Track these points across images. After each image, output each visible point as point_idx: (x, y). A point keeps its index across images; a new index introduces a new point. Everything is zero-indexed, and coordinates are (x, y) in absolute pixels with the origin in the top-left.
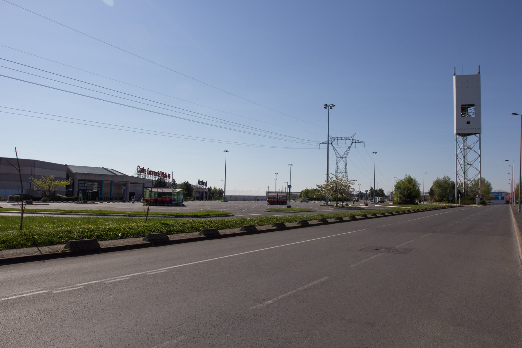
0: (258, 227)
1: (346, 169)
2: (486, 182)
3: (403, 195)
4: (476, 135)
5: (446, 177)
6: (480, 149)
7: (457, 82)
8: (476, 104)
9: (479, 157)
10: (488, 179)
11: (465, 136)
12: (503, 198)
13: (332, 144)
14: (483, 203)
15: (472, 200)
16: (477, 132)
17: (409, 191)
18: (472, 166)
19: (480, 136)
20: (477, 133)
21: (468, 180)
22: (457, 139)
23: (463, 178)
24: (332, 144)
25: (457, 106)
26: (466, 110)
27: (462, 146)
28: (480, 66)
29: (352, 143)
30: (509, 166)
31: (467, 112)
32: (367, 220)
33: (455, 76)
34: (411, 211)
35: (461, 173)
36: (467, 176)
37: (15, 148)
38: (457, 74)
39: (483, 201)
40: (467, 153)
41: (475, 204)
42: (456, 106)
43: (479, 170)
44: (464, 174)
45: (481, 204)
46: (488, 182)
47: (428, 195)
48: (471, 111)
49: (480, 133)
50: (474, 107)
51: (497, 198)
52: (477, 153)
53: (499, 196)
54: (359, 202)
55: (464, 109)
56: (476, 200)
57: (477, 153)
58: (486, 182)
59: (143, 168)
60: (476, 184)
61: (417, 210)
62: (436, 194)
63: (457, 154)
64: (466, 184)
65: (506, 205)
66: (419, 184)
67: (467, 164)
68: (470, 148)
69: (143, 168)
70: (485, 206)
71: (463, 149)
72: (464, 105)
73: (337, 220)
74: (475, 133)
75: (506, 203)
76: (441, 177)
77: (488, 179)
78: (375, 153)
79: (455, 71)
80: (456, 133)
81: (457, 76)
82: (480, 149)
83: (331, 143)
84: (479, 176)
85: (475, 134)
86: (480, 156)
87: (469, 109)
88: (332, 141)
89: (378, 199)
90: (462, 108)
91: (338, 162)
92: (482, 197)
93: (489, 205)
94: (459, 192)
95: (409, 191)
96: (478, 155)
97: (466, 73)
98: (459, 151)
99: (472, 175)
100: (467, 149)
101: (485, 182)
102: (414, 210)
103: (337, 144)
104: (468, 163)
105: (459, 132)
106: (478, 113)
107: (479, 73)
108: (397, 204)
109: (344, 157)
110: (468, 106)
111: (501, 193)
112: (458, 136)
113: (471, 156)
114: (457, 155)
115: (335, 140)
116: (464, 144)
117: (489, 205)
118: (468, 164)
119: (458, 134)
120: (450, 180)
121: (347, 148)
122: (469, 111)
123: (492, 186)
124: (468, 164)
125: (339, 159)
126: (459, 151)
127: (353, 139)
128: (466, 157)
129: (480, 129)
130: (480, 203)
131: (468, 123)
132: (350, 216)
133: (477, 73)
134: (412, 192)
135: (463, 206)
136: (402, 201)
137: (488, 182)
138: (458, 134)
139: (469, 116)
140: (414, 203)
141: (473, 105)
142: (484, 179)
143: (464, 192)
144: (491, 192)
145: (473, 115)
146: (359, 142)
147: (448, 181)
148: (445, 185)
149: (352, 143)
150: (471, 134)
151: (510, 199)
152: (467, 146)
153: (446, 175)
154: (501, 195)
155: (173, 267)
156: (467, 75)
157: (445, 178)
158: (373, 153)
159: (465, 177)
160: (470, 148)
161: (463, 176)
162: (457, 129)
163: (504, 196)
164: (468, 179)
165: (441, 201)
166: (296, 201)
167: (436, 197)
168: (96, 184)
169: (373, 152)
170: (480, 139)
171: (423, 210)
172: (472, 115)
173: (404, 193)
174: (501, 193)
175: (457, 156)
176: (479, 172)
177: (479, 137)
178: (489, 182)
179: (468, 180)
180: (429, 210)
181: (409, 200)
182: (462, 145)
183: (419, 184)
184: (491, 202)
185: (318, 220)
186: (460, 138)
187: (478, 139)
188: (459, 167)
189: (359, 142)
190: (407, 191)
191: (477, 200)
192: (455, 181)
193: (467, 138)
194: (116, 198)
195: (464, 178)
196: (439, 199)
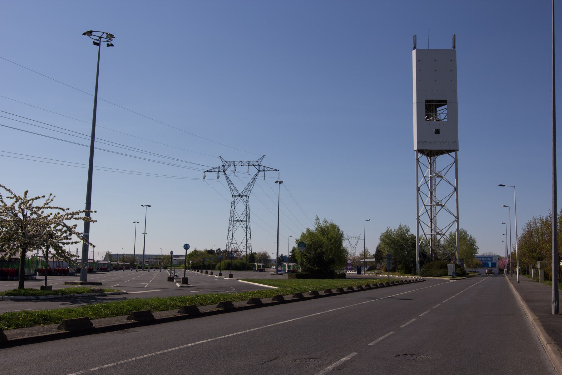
0: (321, 292)
1: (247, 215)
2: (468, 238)
5: (403, 227)
6: (457, 177)
7: (418, 60)
9: (455, 193)
10: (472, 233)
12: (494, 265)
13: (225, 173)
14: (461, 273)
15: (442, 270)
17: (318, 251)
18: (444, 207)
19: (456, 155)
20: (451, 149)
21: (438, 233)
24: (225, 173)
25: (418, 103)
26: (434, 110)
27: (427, 172)
28: (455, 36)
29: (259, 171)
30: (504, 206)
34: (363, 287)
35: (425, 219)
36: (436, 225)
38: (418, 48)
39: (462, 271)
40: (436, 186)
41: (446, 275)
43: (456, 215)
44: (431, 221)
45: (458, 275)
46: (472, 238)
47: (374, 260)
48: (442, 112)
49: (455, 151)
51: (485, 265)
52: (452, 185)
53: (488, 261)
54: (265, 272)
57: (452, 185)
58: (468, 238)
59: (172, 252)
60: (451, 241)
61: (391, 283)
63: (419, 186)
64: (434, 239)
65: (499, 278)
67: (435, 204)
68: (441, 177)
69: (172, 252)
70: (465, 281)
71: (429, 178)
73: (349, 289)
74: (448, 149)
75: (499, 274)
76: (394, 227)
78: (280, 183)
80: (416, 149)
82: (457, 177)
83: (224, 171)
84: (453, 229)
85: (449, 151)
86: (456, 190)
87: (438, 109)
88: (226, 167)
89: (289, 267)
90: (426, 104)
91: (236, 204)
92: (461, 263)
93: (473, 276)
94: (423, 254)
95: (318, 251)
96: (454, 188)
97: (434, 46)
98: (422, 181)
100: (436, 176)
102: (375, 285)
103: (234, 173)
105: (419, 149)
106: (453, 116)
107: (454, 47)
109: (245, 195)
110: (437, 102)
111: (492, 258)
112: (419, 155)
114: (419, 187)
115: (230, 165)
116: (431, 169)
117: (473, 276)
118: (438, 204)
119: (420, 151)
121: (249, 180)
123: (478, 244)
124: (438, 204)
125: (236, 198)
126: (422, 181)
127: (259, 165)
129: (456, 142)
130: (454, 275)
131: (437, 132)
132: (221, 303)
133: (450, 48)
134: (324, 253)
135: (425, 280)
137: (471, 237)
138: (420, 151)
140: (332, 275)
142: (466, 233)
144: (476, 255)
145: (444, 119)
146: (270, 170)
147: (405, 234)
149: (259, 171)
151: (504, 266)
153: (403, 224)
154: (492, 261)
157: (400, 228)
159: (434, 227)
161: (430, 225)
162: (418, 142)
163: (496, 262)
164: (438, 231)
166: (160, 271)
169: (276, 181)
170: (456, 161)
171: (399, 283)
172: (443, 120)
174: (491, 257)
175: (418, 189)
176: (455, 219)
178: (474, 236)
179: (438, 233)
180: (386, 286)
182: (428, 170)
184: (478, 272)
185: (127, 316)
186: (424, 159)
187: (454, 160)
188: (422, 210)
189: (270, 170)
190: (315, 250)
191: (451, 267)
192: (415, 234)
193: (436, 159)
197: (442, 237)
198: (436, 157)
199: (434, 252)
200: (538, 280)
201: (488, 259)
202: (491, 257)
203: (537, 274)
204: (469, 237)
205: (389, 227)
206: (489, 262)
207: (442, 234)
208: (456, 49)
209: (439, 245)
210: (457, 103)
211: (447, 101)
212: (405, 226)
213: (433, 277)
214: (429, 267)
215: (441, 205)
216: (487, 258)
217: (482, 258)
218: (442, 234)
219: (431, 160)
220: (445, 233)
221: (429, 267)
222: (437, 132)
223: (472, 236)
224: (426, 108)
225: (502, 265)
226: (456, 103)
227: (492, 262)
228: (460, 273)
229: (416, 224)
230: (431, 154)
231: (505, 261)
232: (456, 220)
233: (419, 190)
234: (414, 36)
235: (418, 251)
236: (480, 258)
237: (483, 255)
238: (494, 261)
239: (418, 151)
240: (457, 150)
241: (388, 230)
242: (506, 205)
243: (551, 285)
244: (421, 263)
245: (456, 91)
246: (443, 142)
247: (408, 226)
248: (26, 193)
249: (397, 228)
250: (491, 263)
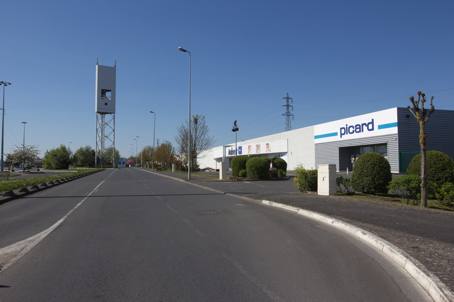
3: (60, 161)
4: (111, 114)
5: (88, 146)
7: (99, 70)
8: (112, 90)
9: (113, 132)
11: (103, 114)
12: (124, 163)
15: (109, 165)
16: (112, 112)
17: (65, 158)
20: (112, 112)
31: (105, 95)
33: (97, 65)
35: (99, 143)
37: (323, 180)
38: (100, 64)
40: (105, 128)
41: (112, 167)
48: (108, 94)
49: (114, 113)
50: (110, 92)
55: (103, 92)
56: (113, 164)
62: (79, 160)
66: (72, 152)
67: (104, 137)
68: (107, 124)
72: (103, 90)
74: (111, 112)
76: (84, 147)
77: (118, 148)
78: (25, 123)
79: (98, 61)
80: (96, 111)
81: (99, 65)
85: (110, 113)
86: (114, 130)
87: (106, 93)
94: (98, 159)
95: (65, 158)
96: (113, 130)
97: (105, 65)
99: (108, 144)
104: (105, 135)
106: (113, 97)
107: (115, 66)
108: (54, 169)
112: (98, 114)
113: (108, 130)
118: (105, 136)
119: (98, 112)
120: (91, 149)
122: (106, 95)
124: (105, 136)
126: (98, 125)
129: (114, 110)
131: (106, 104)
133: (114, 66)
136: (59, 167)
137: (117, 151)
138: (98, 112)
139: (107, 99)
141: (110, 91)
143: (102, 159)
148: (87, 153)
150: (108, 113)
152: (104, 122)
153: (88, 145)
154: (123, 161)
156: (107, 66)
157: (87, 147)
158: (23, 123)
160: (107, 124)
164: (105, 148)
165: (83, 166)
167: (79, 163)
170: (114, 118)
173: (60, 159)
175: (97, 129)
176: (113, 143)
177: (113, 116)
181: (64, 165)
183: (72, 152)
186: (100, 116)
194: (316, 166)
195: (102, 147)
196: (81, 165)
200: (147, 168)
203: (147, 166)
208: (116, 67)
210: (115, 92)
212: (89, 146)
219: (102, 116)
222: (106, 104)
223: (118, 150)
224: (102, 93)
226: (115, 92)
230: (103, 113)
243: (188, 173)
245: (115, 86)
248: (347, 125)
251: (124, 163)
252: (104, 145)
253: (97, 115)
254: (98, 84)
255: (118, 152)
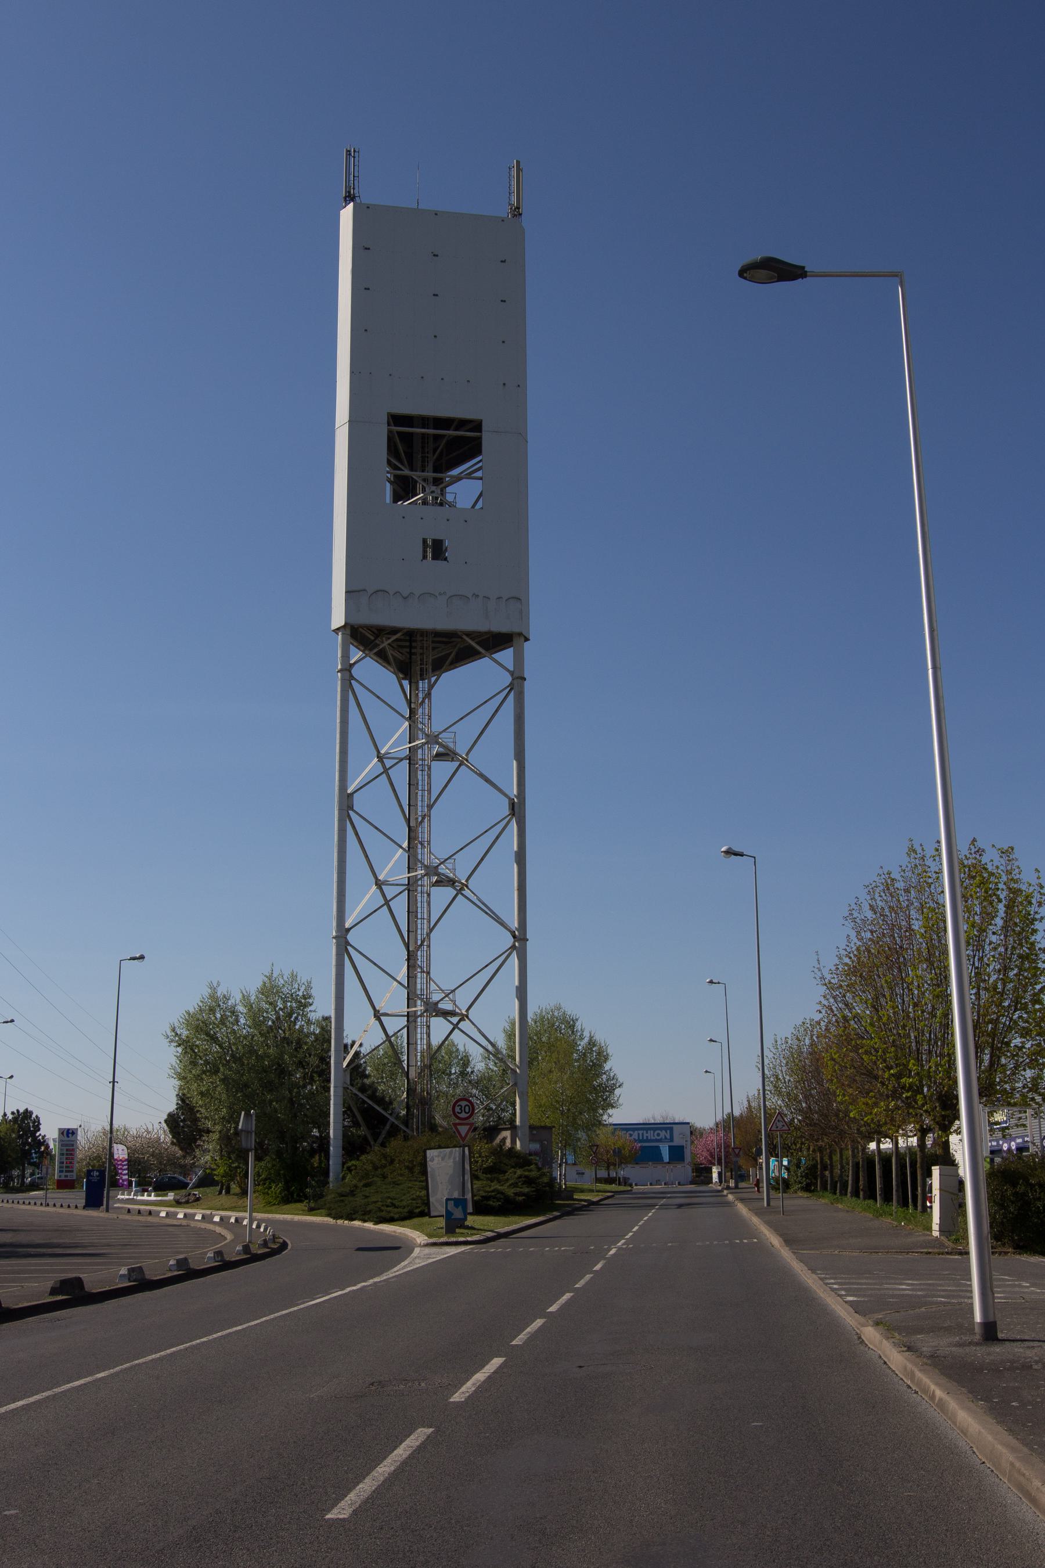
2: (583, 1043)
7: (360, 248)
19: (519, 659)
22: (355, 671)
23: (405, 992)
30: (729, 852)
32: (148, 1294)
36: (428, 973)
38: (365, 199)
39: (529, 1181)
42: (351, 422)
43: (515, 924)
44: (411, 958)
51: (647, 1155)
53: (660, 1141)
80: (343, 623)
86: (517, 809)
90: (390, 432)
96: (507, 801)
101: (573, 1045)
105: (350, 589)
111: (671, 1129)
112: (356, 655)
128: (422, 833)
131: (437, 550)
133: (504, 211)
137: (592, 1043)
142: (571, 1024)
153: (283, 969)
154: (671, 1139)
155: (272, 1316)
157: (269, 990)
161: (402, 974)
162: (348, 592)
168: (453, 1202)
170: (518, 680)
174: (668, 1127)
175: (347, 803)
178: (600, 1037)
187: (508, 679)
197: (456, 1026)
198: (433, 679)
199: (418, 1101)
201: (658, 1135)
202: (668, 1128)
204: (586, 1040)
205: (219, 984)
206: (661, 1145)
207: (453, 1014)
209: (463, 1074)
211: (484, 428)
212: (294, 977)
213: (376, 1223)
214: (376, 1168)
215: (451, 882)
216: (654, 1129)
217: (641, 1132)
218: (453, 1014)
220: (468, 1010)
221: (376, 1168)
225: (705, 1154)
227: (671, 1144)
228: (516, 1194)
229: (334, 962)
231: (714, 1140)
232: (513, 947)
233: (351, 807)
234: (348, 152)
235: (341, 1091)
236: (634, 1130)
237: (645, 1122)
238: (677, 1141)
239: (348, 631)
240: (520, 634)
241: (213, 997)
242: (736, 849)
244: (353, 1148)
245: (521, 386)
246: (461, 596)
247: (303, 977)
249: (253, 985)
250: (670, 1147)
251: (678, 1154)
252: (429, 965)
253: (346, 656)
254: (352, 372)
255: (599, 1053)
